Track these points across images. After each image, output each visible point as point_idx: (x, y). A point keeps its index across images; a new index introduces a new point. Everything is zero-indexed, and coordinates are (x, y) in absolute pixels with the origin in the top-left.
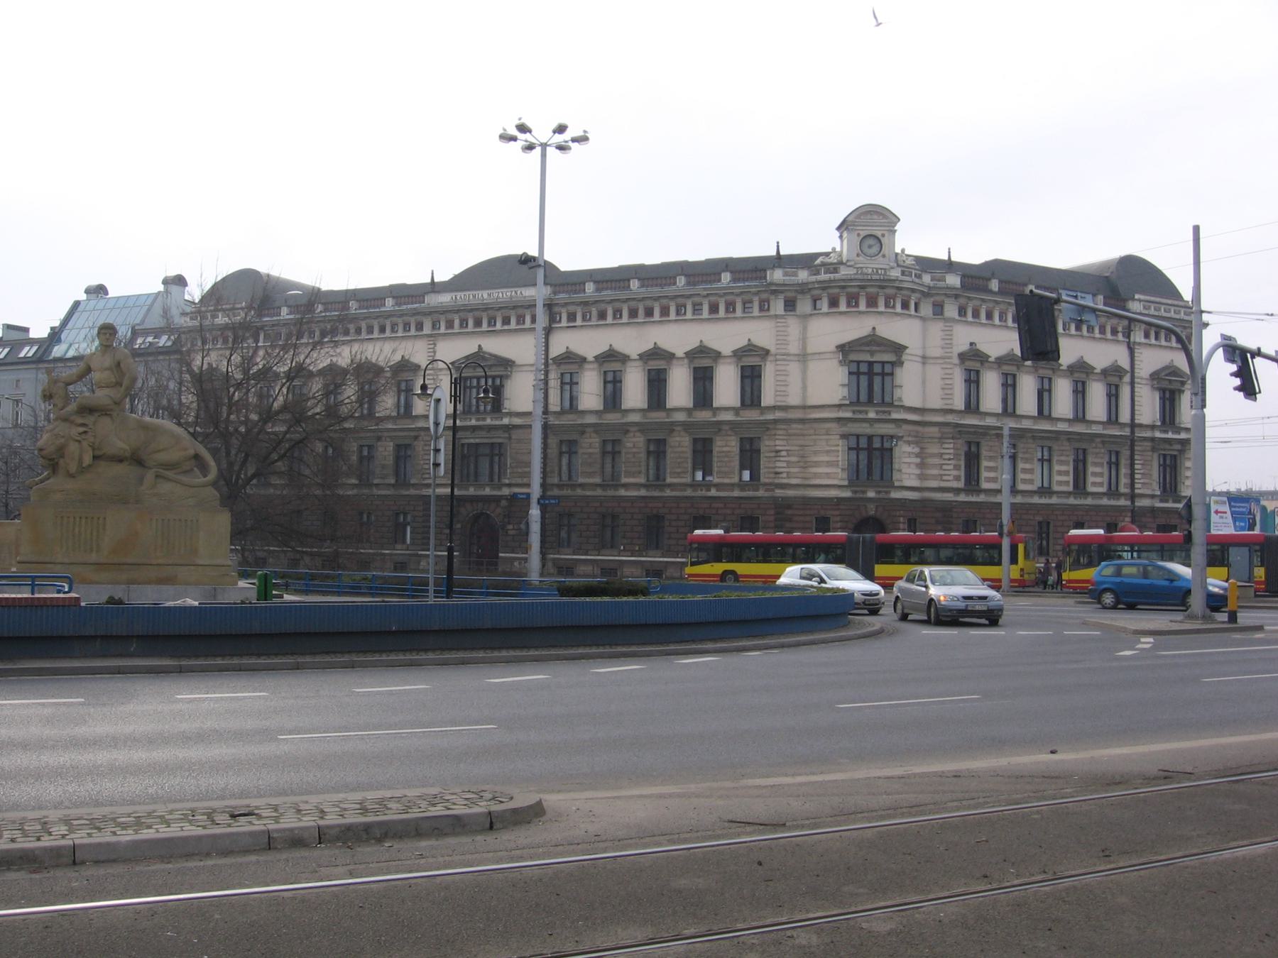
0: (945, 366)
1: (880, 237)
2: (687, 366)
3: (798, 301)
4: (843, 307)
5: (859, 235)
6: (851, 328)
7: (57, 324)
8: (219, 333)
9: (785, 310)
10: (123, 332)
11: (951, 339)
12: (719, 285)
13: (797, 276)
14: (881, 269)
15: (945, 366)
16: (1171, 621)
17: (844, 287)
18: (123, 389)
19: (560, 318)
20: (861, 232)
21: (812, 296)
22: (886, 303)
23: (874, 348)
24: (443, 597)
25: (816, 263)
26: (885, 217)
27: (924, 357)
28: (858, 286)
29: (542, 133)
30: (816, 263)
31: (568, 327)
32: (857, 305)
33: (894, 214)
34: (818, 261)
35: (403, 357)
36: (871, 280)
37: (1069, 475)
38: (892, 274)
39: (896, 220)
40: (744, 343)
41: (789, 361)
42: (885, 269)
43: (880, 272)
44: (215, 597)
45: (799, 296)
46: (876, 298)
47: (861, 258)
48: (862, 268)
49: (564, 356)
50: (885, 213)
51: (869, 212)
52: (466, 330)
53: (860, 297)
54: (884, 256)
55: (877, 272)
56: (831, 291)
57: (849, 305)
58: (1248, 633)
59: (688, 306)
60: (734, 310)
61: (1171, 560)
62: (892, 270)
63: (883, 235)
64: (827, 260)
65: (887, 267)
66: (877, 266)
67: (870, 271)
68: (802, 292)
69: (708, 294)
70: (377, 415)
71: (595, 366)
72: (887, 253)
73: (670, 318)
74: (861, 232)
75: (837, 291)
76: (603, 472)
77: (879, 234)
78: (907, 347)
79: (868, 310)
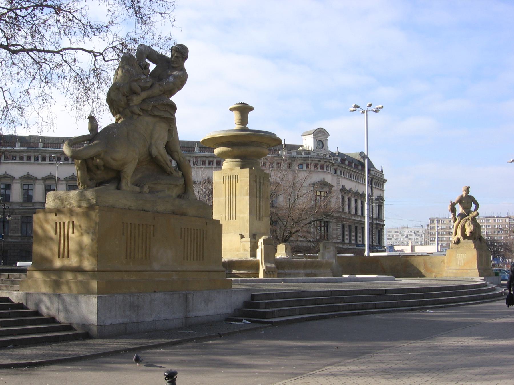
2: (43, 184)
5: (316, 140)
6: (317, 177)
9: (216, 165)
16: (238, 182)
24: (237, 282)
26: (325, 134)
29: (364, 106)
31: (72, 164)
33: (328, 133)
37: (252, 256)
40: (48, 174)
44: (19, 275)
49: (4, 176)
50: (325, 132)
51: (320, 131)
58: (229, 368)
59: (39, 157)
60: (38, 160)
65: (326, 154)
66: (323, 153)
71: (19, 181)
73: (206, 166)
78: (333, 186)
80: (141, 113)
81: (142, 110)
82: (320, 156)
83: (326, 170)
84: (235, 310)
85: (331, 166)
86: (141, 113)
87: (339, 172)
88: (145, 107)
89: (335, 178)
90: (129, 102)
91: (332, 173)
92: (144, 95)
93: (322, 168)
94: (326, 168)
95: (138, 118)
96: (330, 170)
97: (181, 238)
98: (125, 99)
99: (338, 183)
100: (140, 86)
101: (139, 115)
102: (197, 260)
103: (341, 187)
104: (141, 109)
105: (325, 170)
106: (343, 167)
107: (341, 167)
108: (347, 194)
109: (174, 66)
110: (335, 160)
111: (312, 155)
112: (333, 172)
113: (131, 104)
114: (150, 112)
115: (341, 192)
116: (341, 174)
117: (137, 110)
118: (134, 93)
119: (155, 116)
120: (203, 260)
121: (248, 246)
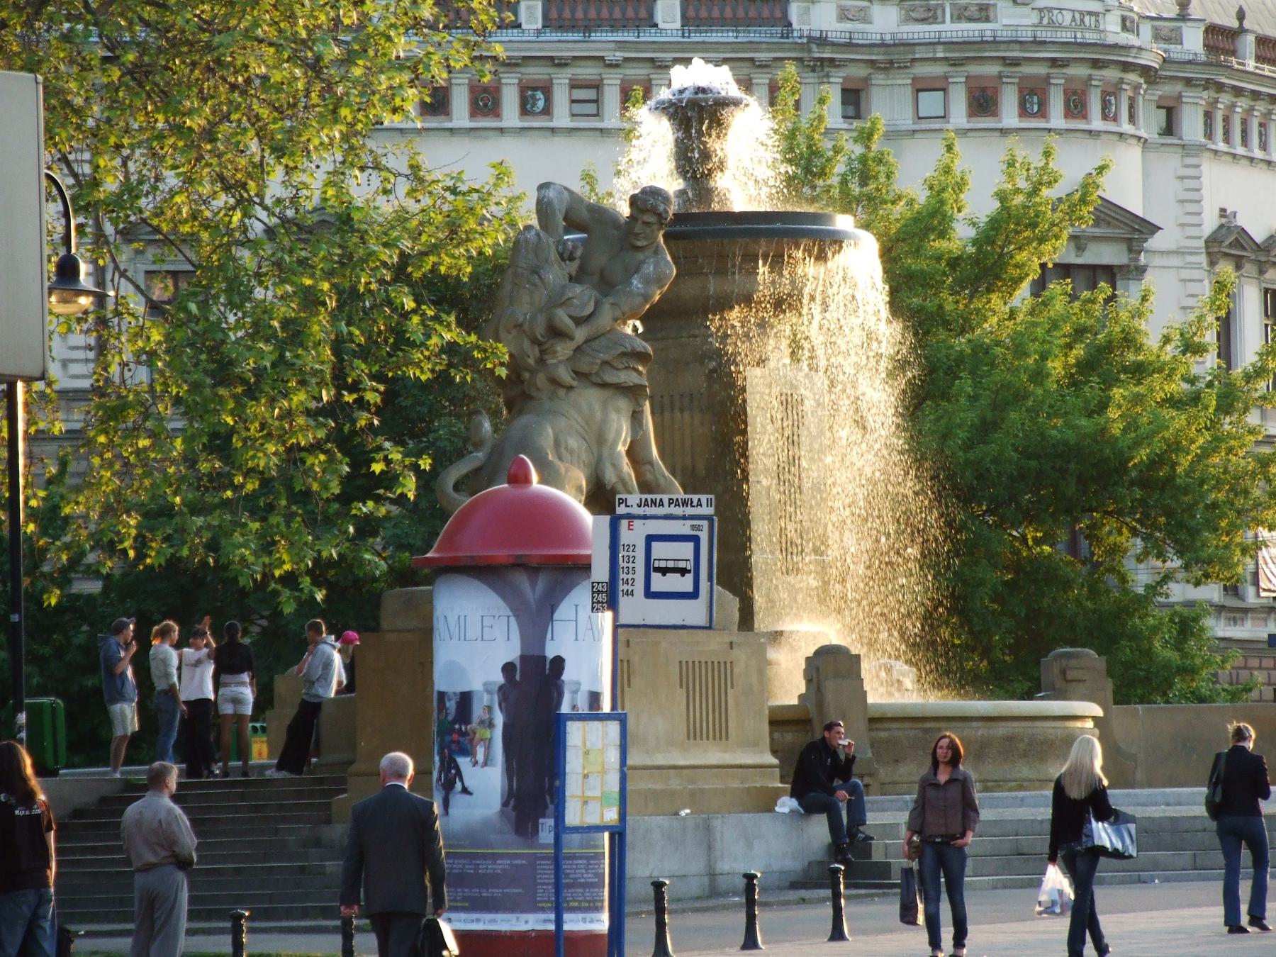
0: (1186, 274)
3: (606, 88)
4: (1009, 116)
8: (406, 76)
11: (1199, 201)
12: (647, 36)
13: (867, 20)
15: (1186, 274)
17: (1015, 62)
18: (576, 264)
19: (548, 100)
21: (915, 79)
22: (1104, 109)
28: (868, 61)
32: (1043, 113)
35: (1002, 197)
45: (879, 79)
46: (1084, 93)
52: (1042, 124)
53: (1053, 90)
55: (1082, 20)
56: (975, 69)
57: (1024, 112)
61: (47, 877)
68: (889, 67)
69: (626, 60)
70: (382, 388)
75: (993, 69)
78: (1154, 229)
79: (526, 124)
80: (575, 383)
81: (578, 374)
82: (1060, 26)
83: (1105, 117)
84: (810, 863)
85: (1137, 88)
86: (575, 383)
87: (1191, 126)
88: (584, 368)
89: (1171, 163)
90: (545, 357)
91: (1142, 133)
92: (580, 334)
93: (1076, 107)
94: (1105, 106)
95: (567, 393)
96: (1132, 118)
97: (681, 686)
98: (537, 350)
99: (1191, 200)
100: (570, 317)
101: (571, 388)
102: (714, 738)
103: (1210, 223)
104: (575, 372)
105: (1097, 124)
106: (1220, 87)
107: (1208, 84)
108: (1249, 268)
109: (639, 244)
110: (1168, 40)
111: (1005, 22)
112: (1150, 123)
113: (551, 361)
114: (594, 379)
115: (1212, 263)
116: (1209, 134)
117: (564, 375)
118: (556, 333)
119: (604, 385)
120: (727, 738)
121: (829, 697)
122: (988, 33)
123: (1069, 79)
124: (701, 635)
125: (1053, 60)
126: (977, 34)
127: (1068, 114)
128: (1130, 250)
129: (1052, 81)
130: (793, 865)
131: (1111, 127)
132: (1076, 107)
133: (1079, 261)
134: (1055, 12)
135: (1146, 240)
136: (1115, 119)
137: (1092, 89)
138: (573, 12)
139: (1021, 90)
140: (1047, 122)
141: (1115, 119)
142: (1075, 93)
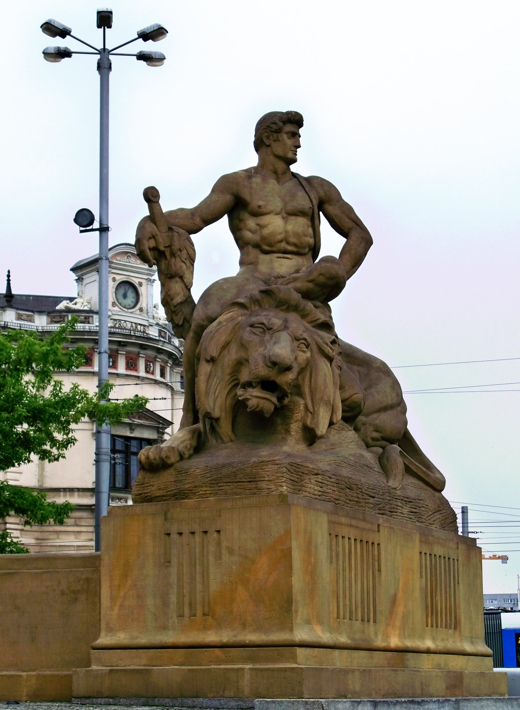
1: (137, 286)
7: (94, 480)
10: (309, 443)
14: (141, 325)
20: (118, 277)
22: (146, 369)
23: (137, 421)
25: (58, 308)
27: (172, 409)
30: (58, 308)
34: (61, 306)
36: (129, 336)
38: (150, 333)
39: (166, 32)
41: (337, 564)
42: (144, 326)
43: (139, 327)
47: (116, 308)
48: (120, 320)
54: (141, 310)
55: (136, 327)
62: (150, 328)
63: (141, 284)
64: (71, 305)
67: (129, 325)
72: (144, 306)
74: (118, 277)
76: (333, 410)
77: (135, 281)
93: (131, 365)
96: (163, 375)
122: (87, 327)
123: (128, 352)
124: (107, 504)
125: (119, 342)
126: (81, 328)
127: (128, 368)
128: (158, 432)
129: (119, 352)
130: (302, 400)
131: (150, 376)
132: (132, 365)
133: (132, 435)
134: (122, 322)
135: (166, 428)
136: (153, 373)
137: (140, 358)
138: (170, 364)
139: (126, 359)
140: (117, 370)
141: (153, 373)
142: (131, 359)
